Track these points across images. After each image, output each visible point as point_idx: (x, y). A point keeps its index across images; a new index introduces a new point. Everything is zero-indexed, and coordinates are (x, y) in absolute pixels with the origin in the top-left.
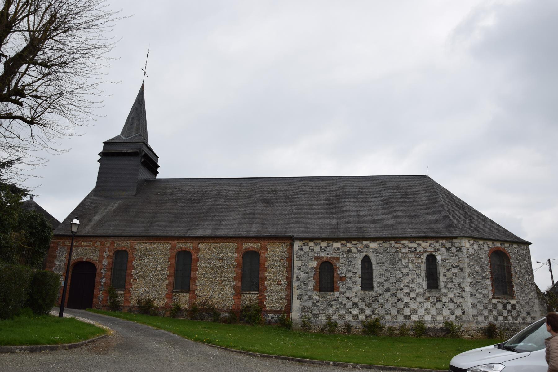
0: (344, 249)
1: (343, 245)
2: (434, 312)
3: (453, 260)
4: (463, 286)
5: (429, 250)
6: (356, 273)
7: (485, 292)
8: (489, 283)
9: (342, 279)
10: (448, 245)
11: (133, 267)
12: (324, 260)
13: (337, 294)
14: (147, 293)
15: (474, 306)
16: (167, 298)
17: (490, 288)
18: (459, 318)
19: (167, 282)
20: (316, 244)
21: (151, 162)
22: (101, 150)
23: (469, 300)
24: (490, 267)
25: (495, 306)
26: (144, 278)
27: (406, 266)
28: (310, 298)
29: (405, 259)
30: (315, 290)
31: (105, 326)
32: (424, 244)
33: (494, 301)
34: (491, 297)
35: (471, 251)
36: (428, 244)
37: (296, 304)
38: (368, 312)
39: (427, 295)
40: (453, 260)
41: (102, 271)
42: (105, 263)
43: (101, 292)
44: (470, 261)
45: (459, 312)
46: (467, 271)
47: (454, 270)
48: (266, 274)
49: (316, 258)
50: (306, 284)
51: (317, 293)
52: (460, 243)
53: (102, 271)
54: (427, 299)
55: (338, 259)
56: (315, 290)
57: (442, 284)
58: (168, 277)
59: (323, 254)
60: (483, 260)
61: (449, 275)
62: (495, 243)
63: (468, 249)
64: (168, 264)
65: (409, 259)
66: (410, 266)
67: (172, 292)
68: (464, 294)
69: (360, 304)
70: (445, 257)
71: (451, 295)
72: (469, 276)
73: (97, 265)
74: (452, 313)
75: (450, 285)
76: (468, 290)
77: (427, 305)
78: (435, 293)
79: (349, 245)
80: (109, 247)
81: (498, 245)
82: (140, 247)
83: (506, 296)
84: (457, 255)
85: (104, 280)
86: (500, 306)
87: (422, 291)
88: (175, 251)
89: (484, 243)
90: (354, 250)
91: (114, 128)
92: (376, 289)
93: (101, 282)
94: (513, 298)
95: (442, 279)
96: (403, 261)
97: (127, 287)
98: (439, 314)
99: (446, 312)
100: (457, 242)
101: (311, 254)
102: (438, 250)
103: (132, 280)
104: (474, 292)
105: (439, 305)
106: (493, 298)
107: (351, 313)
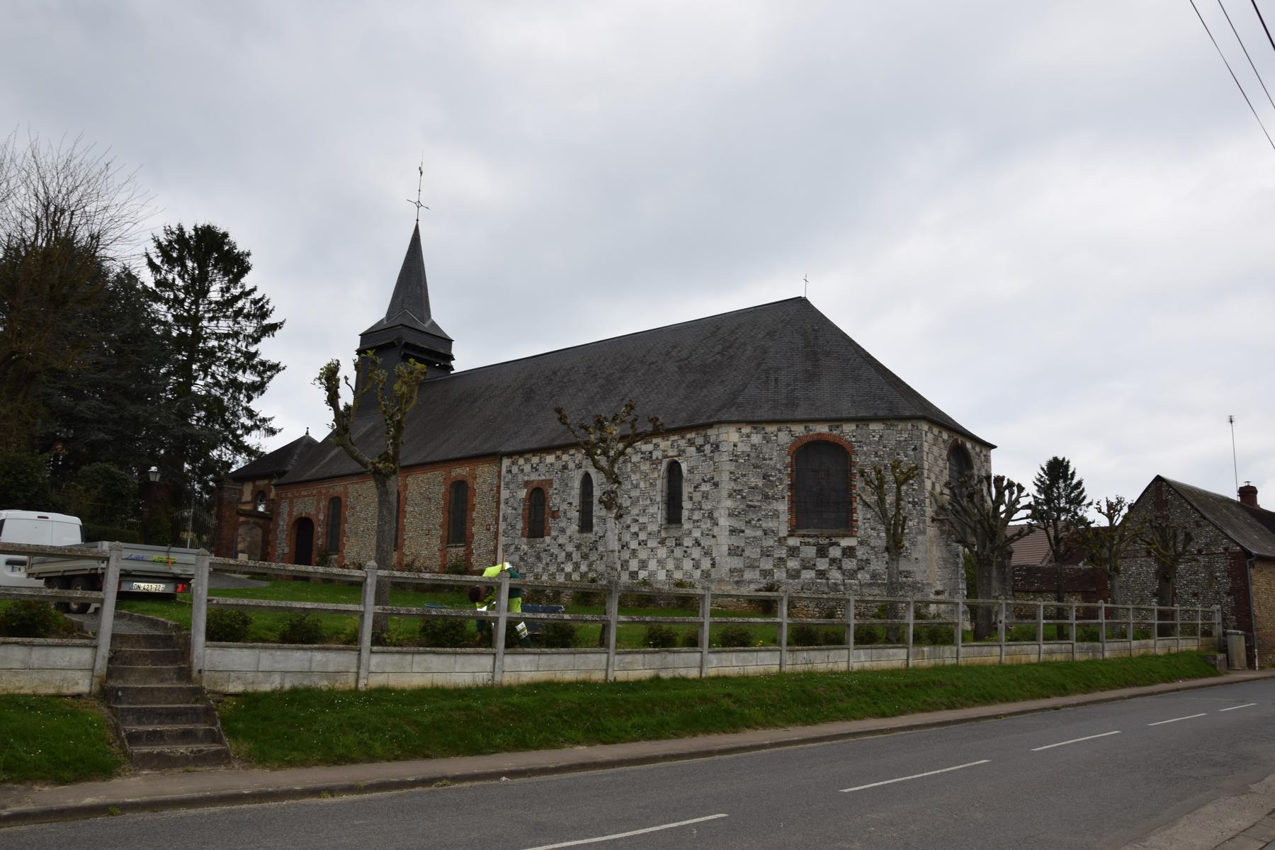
0: (559, 465)
1: (558, 458)
2: (670, 565)
3: (705, 469)
4: (715, 515)
5: (671, 454)
6: (570, 504)
7: (770, 525)
8: (783, 507)
9: (555, 515)
10: (699, 441)
12: (535, 485)
13: (548, 539)
15: (734, 551)
17: (785, 517)
18: (706, 575)
20: (527, 461)
21: (436, 350)
22: (357, 346)
23: (724, 542)
24: (790, 475)
25: (793, 552)
27: (636, 486)
28: (517, 549)
29: (635, 473)
30: (523, 535)
32: (664, 444)
33: (793, 542)
34: (784, 532)
35: (742, 447)
36: (669, 443)
38: (584, 568)
39: (663, 534)
40: (705, 469)
42: (321, 517)
44: (738, 467)
45: (706, 564)
46: (727, 486)
47: (705, 487)
48: (474, 514)
49: (527, 484)
50: (513, 527)
51: (525, 540)
52: (718, 436)
54: (662, 542)
55: (550, 483)
56: (523, 535)
57: (685, 514)
59: (534, 477)
60: (772, 463)
61: (697, 496)
62: (812, 426)
63: (735, 445)
65: (641, 472)
66: (642, 485)
68: (716, 531)
69: (574, 555)
70: (693, 464)
71: (696, 534)
72: (730, 496)
73: (315, 521)
74: (697, 566)
75: (697, 516)
76: (724, 522)
77: (662, 552)
78: (675, 533)
79: (565, 457)
81: (823, 429)
83: (826, 532)
84: (711, 458)
86: (810, 552)
87: (653, 528)
89: (779, 430)
90: (571, 465)
91: (371, 306)
92: (595, 529)
94: (850, 535)
95: (687, 505)
96: (633, 477)
98: (677, 568)
99: (687, 565)
100: (712, 433)
101: (521, 478)
102: (684, 451)
104: (739, 524)
105: (678, 552)
106: (790, 535)
107: (563, 570)
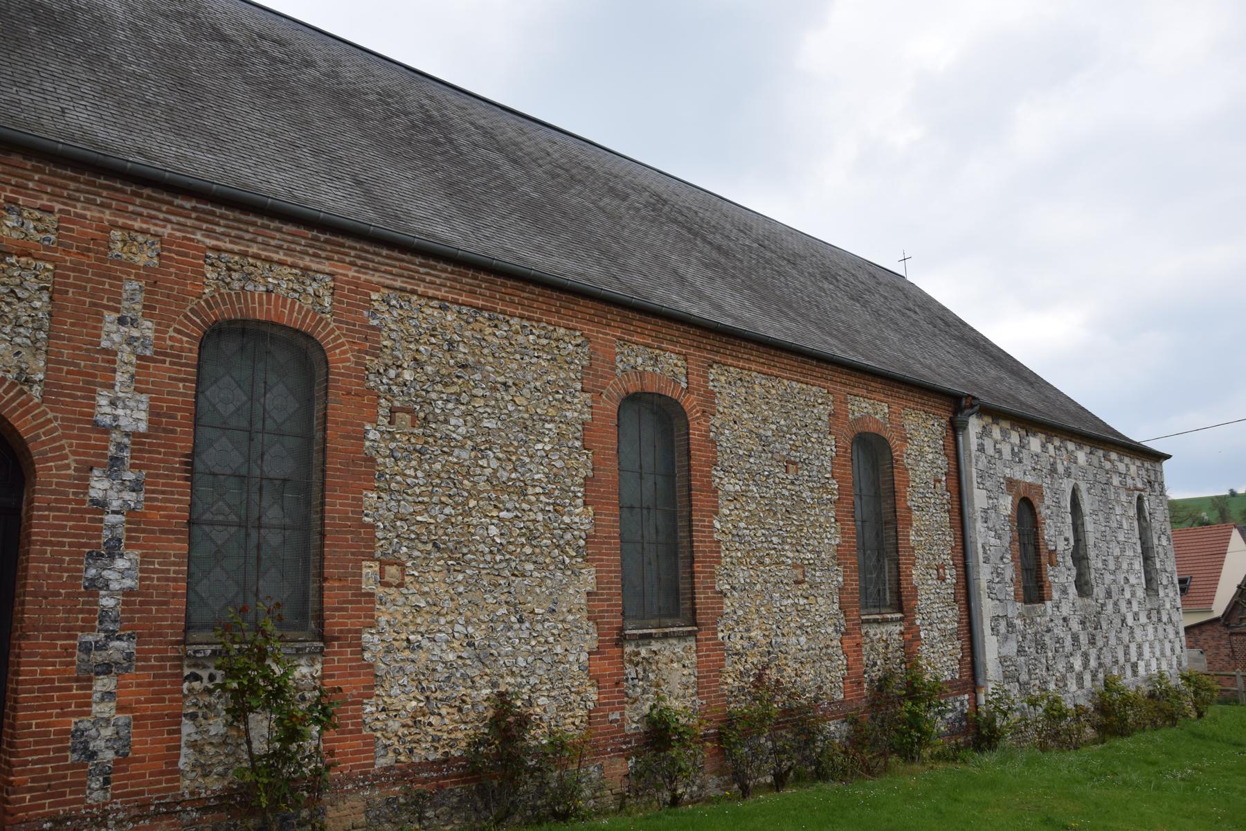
11: (366, 469)
14: (483, 657)
16: (597, 680)
19: (589, 577)
26: (454, 555)
31: (190, 201)
37: (992, 649)
41: (99, 486)
43: (103, 684)
53: (99, 486)
58: (591, 548)
64: (583, 464)
67: (621, 640)
80: (152, 277)
82: (411, 326)
85: (121, 573)
88: (616, 389)
93: (95, 587)
97: (335, 622)
103: (370, 570)
